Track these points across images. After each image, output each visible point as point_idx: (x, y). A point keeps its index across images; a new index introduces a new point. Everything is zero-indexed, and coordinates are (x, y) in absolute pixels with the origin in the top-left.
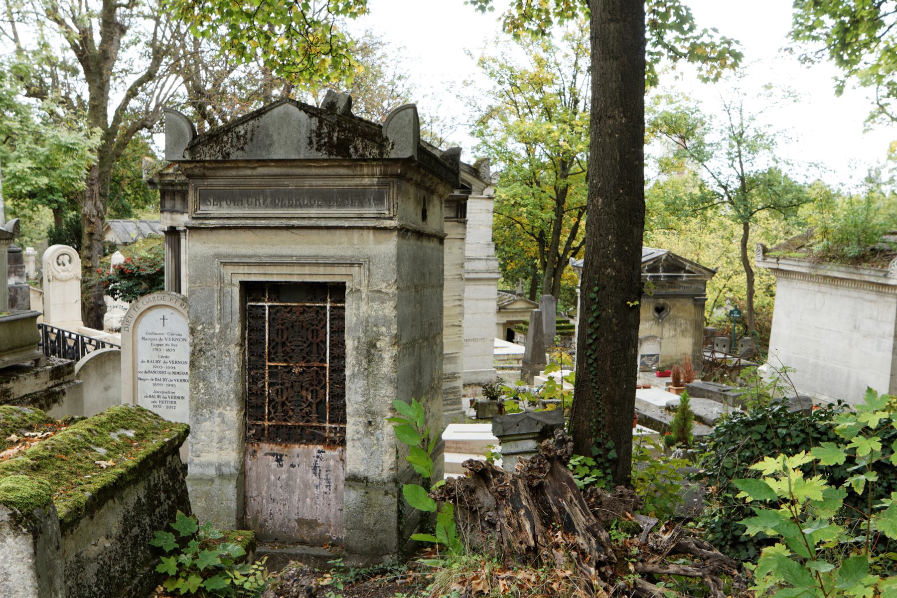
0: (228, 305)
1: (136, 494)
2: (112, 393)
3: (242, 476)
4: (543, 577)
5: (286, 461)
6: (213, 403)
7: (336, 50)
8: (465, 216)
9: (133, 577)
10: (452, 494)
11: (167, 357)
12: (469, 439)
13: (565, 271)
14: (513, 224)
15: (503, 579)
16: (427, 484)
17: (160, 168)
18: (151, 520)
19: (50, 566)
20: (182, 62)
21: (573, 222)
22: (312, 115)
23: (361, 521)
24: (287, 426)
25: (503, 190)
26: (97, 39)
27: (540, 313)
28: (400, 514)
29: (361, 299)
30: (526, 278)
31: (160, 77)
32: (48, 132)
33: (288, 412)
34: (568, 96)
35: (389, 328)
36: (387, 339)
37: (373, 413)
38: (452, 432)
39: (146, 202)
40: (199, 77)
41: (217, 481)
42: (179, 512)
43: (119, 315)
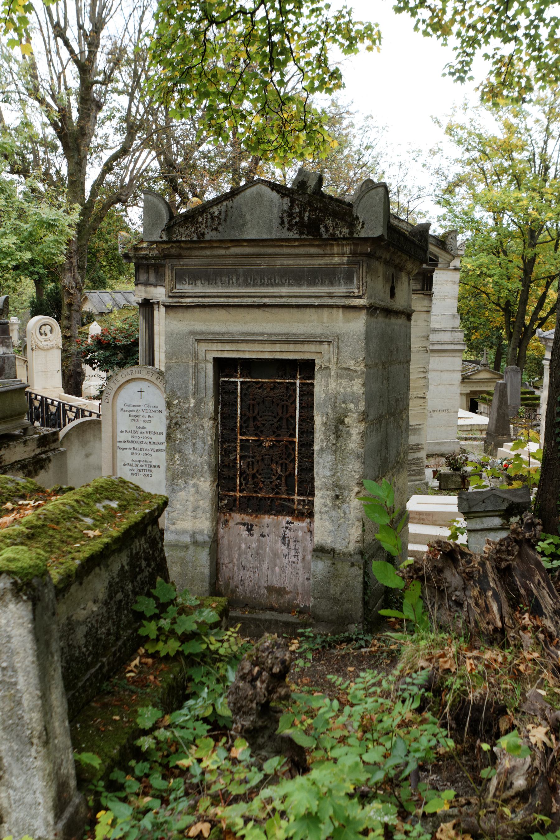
0: (202, 380)
1: (121, 561)
2: (92, 459)
3: (215, 543)
4: (510, 658)
5: (256, 531)
6: (188, 474)
7: (310, 126)
8: (431, 289)
9: (118, 639)
10: (420, 573)
11: (144, 428)
12: (433, 516)
13: (531, 342)
14: (479, 294)
15: (469, 658)
16: (390, 559)
17: (135, 243)
18: (134, 586)
19: (47, 631)
20: (155, 137)
21: (540, 293)
22: (283, 196)
23: (327, 590)
24: (257, 497)
25: (469, 260)
26: (75, 115)
27: (505, 385)
28: (365, 584)
29: (329, 375)
30: (491, 347)
31: (134, 151)
32: (32, 209)
33: (258, 484)
34: (538, 162)
35: (356, 405)
36: (355, 415)
37: (340, 487)
38: (416, 503)
39: (120, 273)
40: (171, 152)
41: (192, 548)
42: (159, 579)
43: (96, 383)
